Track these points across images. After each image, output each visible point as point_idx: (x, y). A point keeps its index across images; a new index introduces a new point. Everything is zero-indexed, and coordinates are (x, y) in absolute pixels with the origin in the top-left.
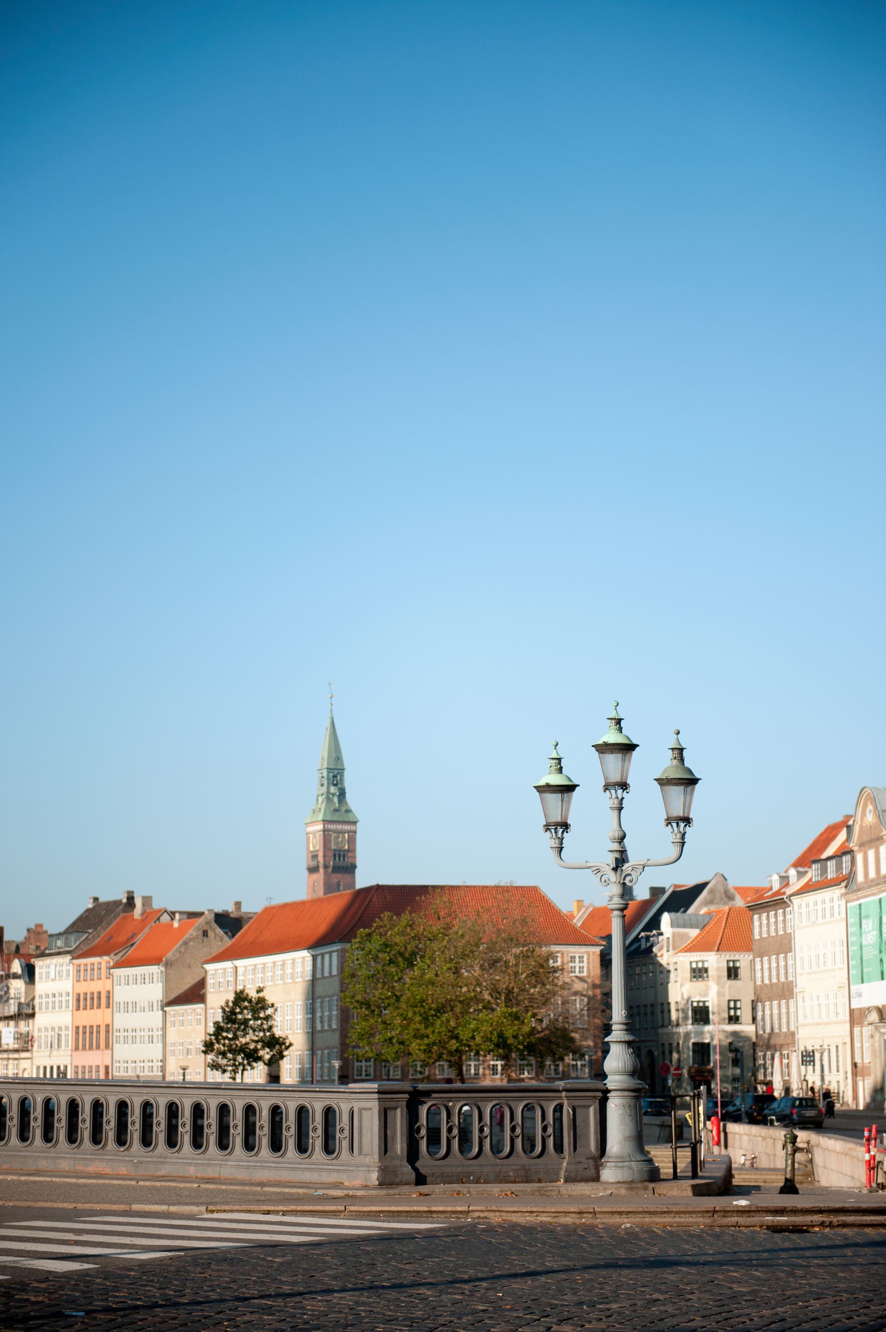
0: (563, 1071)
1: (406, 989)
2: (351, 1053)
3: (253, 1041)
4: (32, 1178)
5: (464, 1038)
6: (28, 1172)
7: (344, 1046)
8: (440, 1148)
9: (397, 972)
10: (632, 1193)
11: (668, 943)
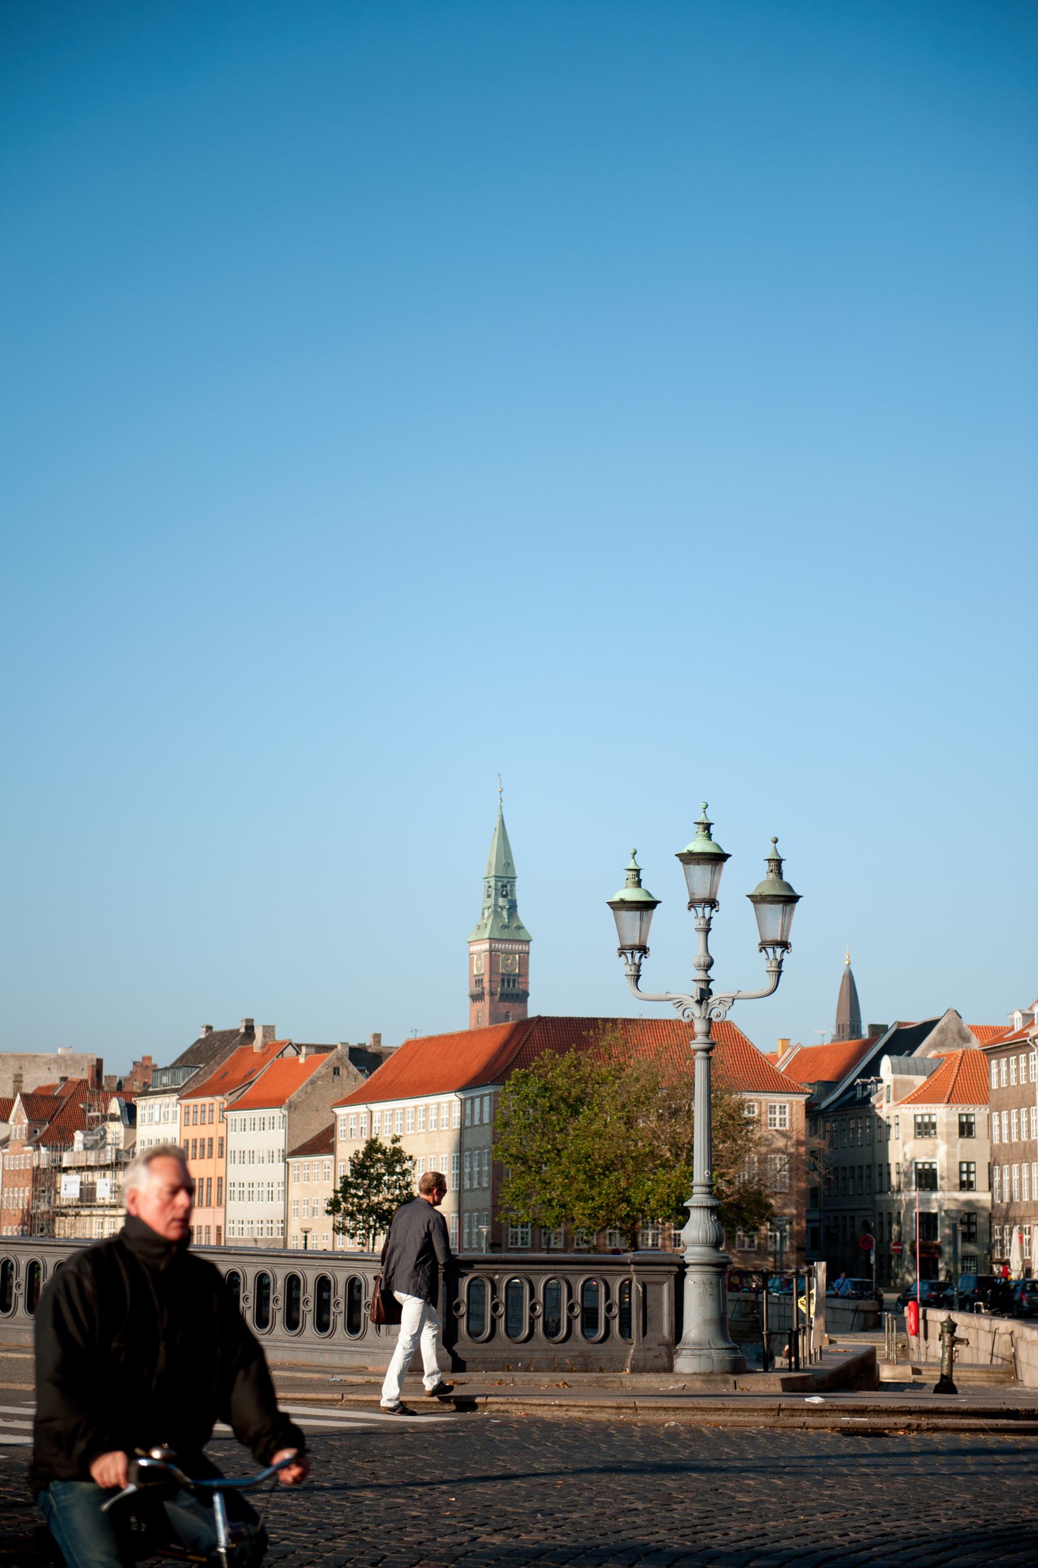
0: (759, 1244)
1: (569, 1141)
2: (503, 1217)
3: (387, 1200)
4: (9, 1355)
5: (637, 1202)
6: (7, 1347)
7: (496, 1208)
8: (596, 1332)
9: (559, 1120)
10: (710, 1387)
11: (888, 1092)
